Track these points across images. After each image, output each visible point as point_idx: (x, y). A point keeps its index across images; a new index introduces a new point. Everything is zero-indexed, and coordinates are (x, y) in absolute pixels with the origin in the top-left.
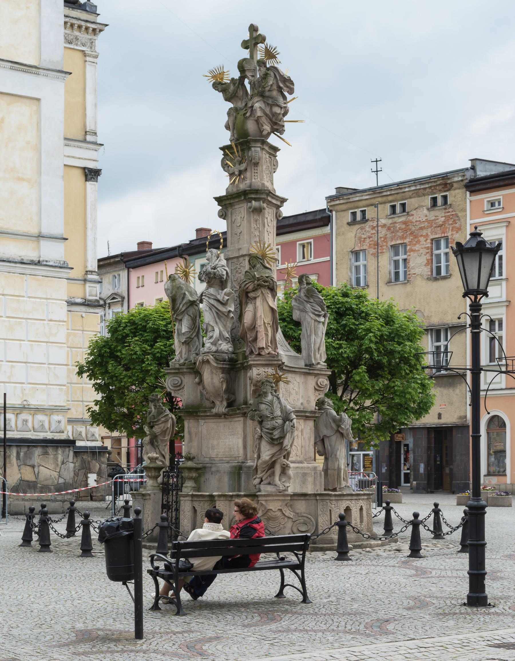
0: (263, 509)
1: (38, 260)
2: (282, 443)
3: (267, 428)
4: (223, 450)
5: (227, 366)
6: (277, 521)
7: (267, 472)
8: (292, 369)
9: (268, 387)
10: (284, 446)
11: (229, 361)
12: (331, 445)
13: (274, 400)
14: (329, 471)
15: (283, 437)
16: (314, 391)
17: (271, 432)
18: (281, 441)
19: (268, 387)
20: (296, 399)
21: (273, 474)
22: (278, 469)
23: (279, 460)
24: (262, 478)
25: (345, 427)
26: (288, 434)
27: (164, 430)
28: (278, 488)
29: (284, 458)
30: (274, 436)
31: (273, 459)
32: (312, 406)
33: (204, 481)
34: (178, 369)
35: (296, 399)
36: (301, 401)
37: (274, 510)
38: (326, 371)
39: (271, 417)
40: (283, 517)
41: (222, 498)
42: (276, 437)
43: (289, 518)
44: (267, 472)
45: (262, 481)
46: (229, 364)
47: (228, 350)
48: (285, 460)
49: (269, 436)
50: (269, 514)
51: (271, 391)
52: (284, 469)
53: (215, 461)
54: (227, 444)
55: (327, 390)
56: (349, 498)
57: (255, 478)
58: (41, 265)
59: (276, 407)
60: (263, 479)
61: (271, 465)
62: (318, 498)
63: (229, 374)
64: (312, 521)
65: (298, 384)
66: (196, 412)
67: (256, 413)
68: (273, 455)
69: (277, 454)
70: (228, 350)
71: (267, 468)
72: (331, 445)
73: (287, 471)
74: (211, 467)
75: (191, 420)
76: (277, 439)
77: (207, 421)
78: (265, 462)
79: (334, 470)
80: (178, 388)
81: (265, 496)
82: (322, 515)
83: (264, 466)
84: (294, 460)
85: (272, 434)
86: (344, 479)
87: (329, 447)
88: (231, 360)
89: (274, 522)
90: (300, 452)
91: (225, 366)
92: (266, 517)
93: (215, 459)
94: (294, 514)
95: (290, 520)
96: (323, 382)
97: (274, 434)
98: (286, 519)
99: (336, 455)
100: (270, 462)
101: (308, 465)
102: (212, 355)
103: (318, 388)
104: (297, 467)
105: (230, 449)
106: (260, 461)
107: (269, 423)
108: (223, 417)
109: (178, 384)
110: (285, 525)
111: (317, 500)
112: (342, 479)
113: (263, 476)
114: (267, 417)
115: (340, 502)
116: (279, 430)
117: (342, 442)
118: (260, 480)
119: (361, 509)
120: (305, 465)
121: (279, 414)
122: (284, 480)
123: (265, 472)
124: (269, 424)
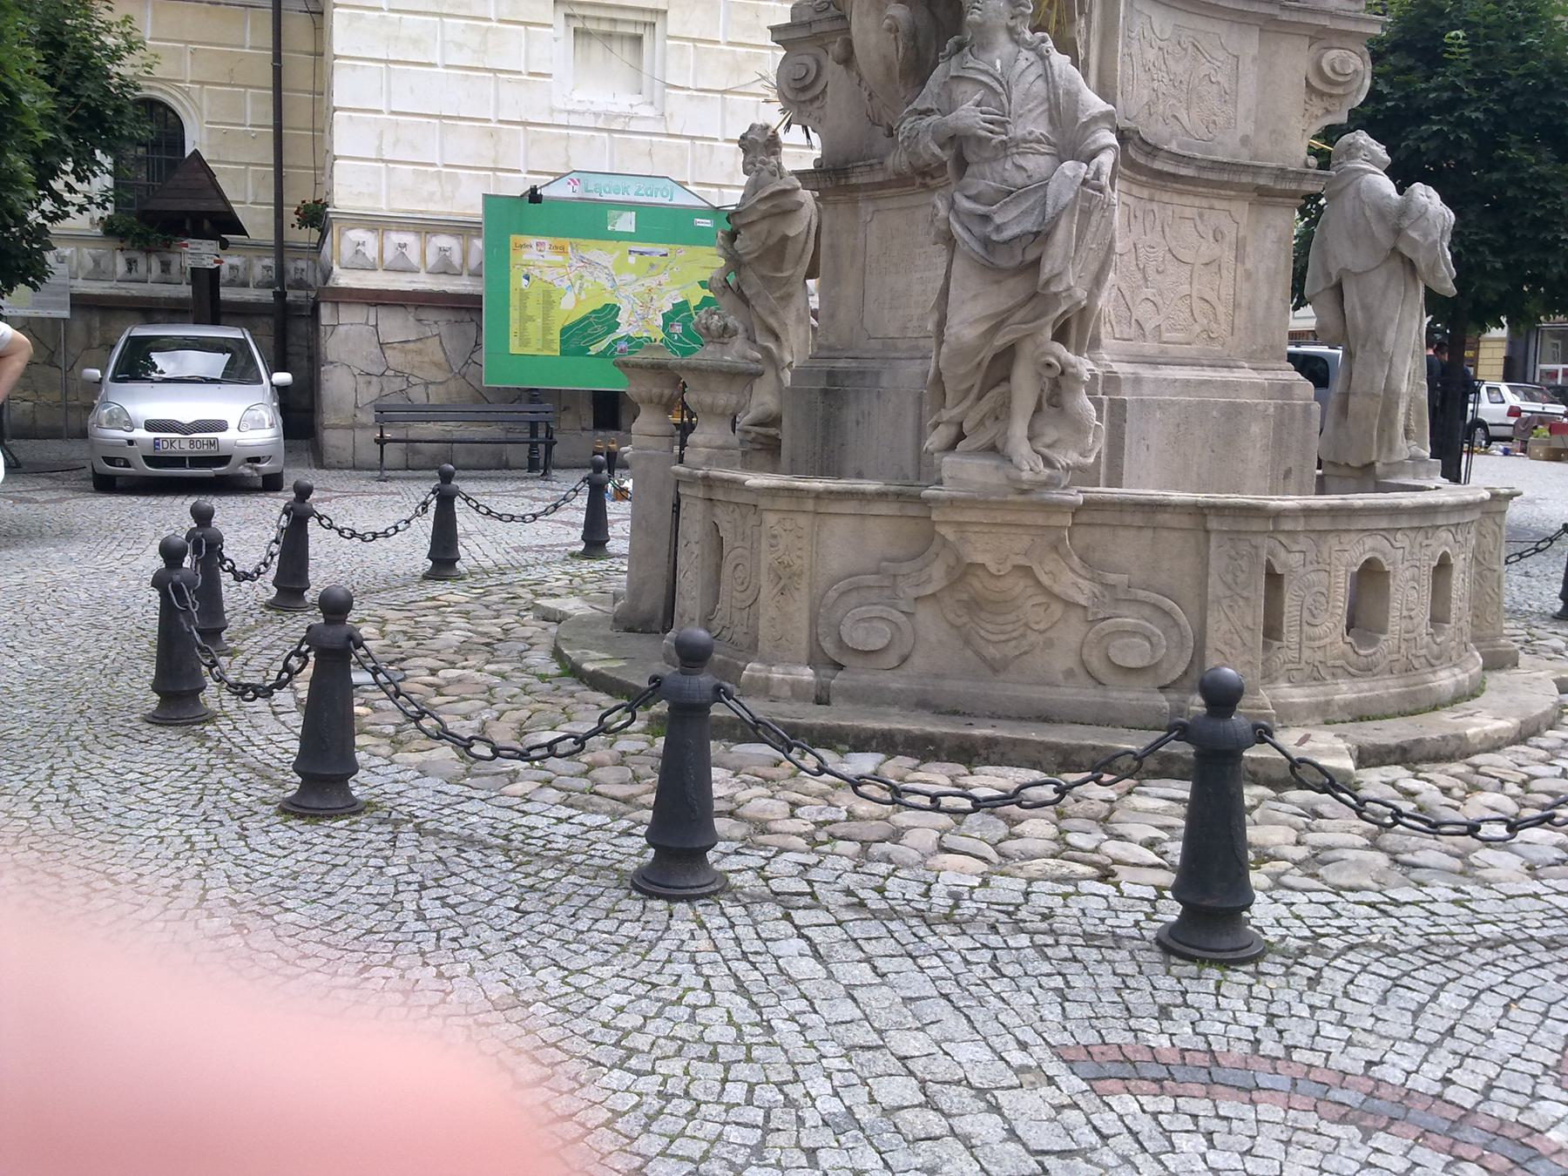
0: (952, 562)
3: (973, 192)
6: (1012, 617)
7: (979, 398)
10: (1044, 276)
12: (1366, 308)
14: (1352, 400)
15: (1041, 236)
16: (1304, 96)
21: (1002, 413)
22: (1024, 387)
23: (1027, 349)
25: (1425, 236)
26: (1063, 223)
27: (771, 242)
28: (1013, 473)
29: (1061, 335)
30: (999, 229)
31: (1001, 341)
32: (1296, 149)
33: (858, 423)
35: (1220, 121)
36: (1246, 127)
37: (993, 569)
38: (1358, 20)
40: (1041, 599)
42: (1007, 234)
43: (1069, 604)
45: (961, 436)
48: (1058, 348)
50: (976, 583)
51: (1006, 19)
52: (1056, 391)
53: (896, 349)
55: (1362, 98)
56: (1384, 523)
57: (936, 426)
59: (1027, 94)
61: (1001, 366)
62: (1213, 524)
64: (1176, 624)
65: (1231, 60)
67: (928, 120)
68: (999, 323)
69: (1018, 316)
71: (978, 380)
72: (1366, 308)
74: (878, 374)
75: (841, 207)
77: (881, 204)
78: (962, 353)
79: (1373, 396)
80: (809, 95)
81: (952, 502)
82: (1225, 603)
83: (962, 370)
84: (1194, 353)
86: (1407, 432)
87: (1359, 313)
89: (1000, 619)
92: (965, 596)
93: (900, 343)
94: (1097, 589)
95: (1075, 618)
96: (1343, 62)
97: (998, 220)
98: (1057, 609)
99: (1380, 343)
100: (987, 354)
101: (1254, 374)
103: (1320, 87)
106: (944, 349)
110: (1050, 634)
111: (1207, 532)
112: (1401, 430)
113: (965, 414)
114: (980, 140)
115: (1332, 541)
117: (1411, 293)
118: (953, 430)
119: (1443, 567)
120: (1245, 375)
121: (1040, 128)
122: (1051, 435)
123: (973, 396)
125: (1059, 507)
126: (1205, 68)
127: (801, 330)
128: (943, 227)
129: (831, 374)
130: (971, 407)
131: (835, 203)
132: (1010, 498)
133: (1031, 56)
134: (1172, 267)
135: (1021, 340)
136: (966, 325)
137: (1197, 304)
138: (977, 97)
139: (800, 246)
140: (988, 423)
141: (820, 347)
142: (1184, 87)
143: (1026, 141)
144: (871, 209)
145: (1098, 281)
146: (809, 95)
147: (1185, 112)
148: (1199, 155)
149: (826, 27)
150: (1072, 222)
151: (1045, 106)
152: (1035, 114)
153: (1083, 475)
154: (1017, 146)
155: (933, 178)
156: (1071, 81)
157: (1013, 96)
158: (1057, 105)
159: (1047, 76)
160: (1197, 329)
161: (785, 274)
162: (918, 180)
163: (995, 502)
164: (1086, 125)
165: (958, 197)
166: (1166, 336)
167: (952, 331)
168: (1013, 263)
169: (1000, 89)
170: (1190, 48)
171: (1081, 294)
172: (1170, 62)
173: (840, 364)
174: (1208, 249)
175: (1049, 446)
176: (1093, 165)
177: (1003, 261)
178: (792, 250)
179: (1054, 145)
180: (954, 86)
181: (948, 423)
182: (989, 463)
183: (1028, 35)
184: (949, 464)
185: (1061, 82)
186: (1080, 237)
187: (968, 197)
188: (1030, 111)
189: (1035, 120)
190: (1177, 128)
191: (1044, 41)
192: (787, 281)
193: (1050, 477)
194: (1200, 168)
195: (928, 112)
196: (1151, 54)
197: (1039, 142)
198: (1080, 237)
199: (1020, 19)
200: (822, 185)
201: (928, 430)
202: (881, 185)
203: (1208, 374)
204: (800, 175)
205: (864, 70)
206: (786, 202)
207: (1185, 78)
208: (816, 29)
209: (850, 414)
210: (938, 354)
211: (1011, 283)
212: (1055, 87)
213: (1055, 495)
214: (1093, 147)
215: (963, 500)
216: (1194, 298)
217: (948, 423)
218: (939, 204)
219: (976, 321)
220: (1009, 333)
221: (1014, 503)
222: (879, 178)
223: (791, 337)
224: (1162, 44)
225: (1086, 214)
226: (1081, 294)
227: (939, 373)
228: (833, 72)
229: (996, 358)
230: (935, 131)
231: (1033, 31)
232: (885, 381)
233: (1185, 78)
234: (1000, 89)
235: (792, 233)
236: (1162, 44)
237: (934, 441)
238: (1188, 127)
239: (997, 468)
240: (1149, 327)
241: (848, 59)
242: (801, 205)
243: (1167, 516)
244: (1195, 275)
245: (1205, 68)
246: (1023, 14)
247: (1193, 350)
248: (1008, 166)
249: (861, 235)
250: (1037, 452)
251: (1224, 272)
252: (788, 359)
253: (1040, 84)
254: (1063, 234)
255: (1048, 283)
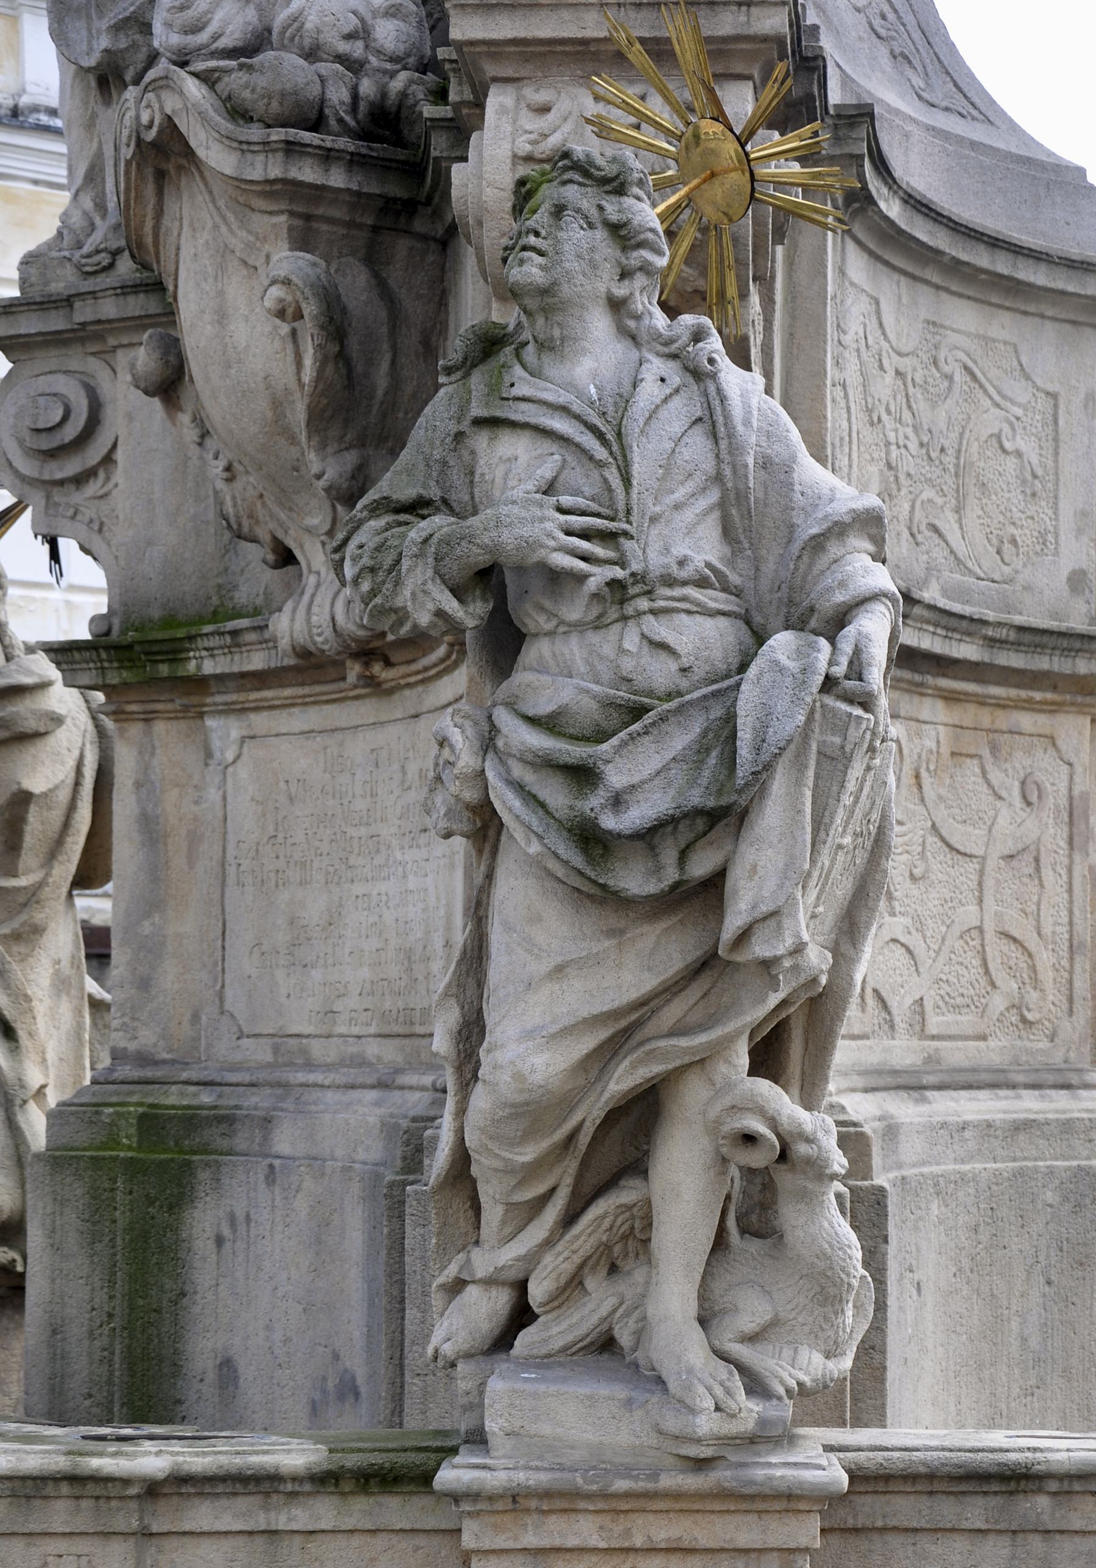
1: (10, 103)
2: (712, 890)
3: (543, 707)
4: (365, 973)
5: (338, 178)
7: (569, 1219)
8: (981, 258)
9: (576, 236)
10: (734, 922)
11: (363, 135)
13: (649, 391)
15: (723, 817)
17: (576, 752)
18: (701, 866)
19: (576, 236)
20: (1026, 536)
21: (632, 1243)
22: (683, 1185)
23: (693, 1102)
24: (521, 1287)
26: (778, 786)
28: (672, 1423)
29: (767, 1058)
30: (617, 802)
31: (624, 1079)
34: (67, 302)
35: (1026, 536)
39: (599, 576)
41: (59, 1514)
42: (638, 815)
44: (569, 1219)
45: (522, 1315)
46: (355, 161)
47: (362, 33)
48: (764, 1086)
49: (556, 794)
51: (606, 282)
53: (310, 1065)
54: (389, 916)
57: (457, 1286)
58: (22, 127)
59: (668, 465)
60: (537, 1292)
63: (373, 259)
65: (1043, 404)
66: (175, 651)
67: (419, 530)
68: (624, 1030)
69: (672, 1013)
70: (362, 33)
71: (565, 1175)
73: (790, 1216)
74: (267, 1121)
76: (648, 837)
77: (260, 721)
78: (531, 1113)
80: (71, 467)
81: (515, 1501)
83: (527, 1154)
85: (583, 776)
88: (384, 123)
90: (1054, 995)
91: (308, 173)
93: (317, 1049)
97: (616, 777)
100: (591, 1112)
102: (207, 79)
104: (1022, 1127)
105: (408, 956)
106: (480, 1100)
107: (573, 649)
108: (354, 671)
109: (70, 432)
113: (533, 1259)
114: (557, 580)
116: (681, 738)
118: (501, 1301)
121: (704, 549)
122: (751, 1310)
123: (552, 1214)
124: (564, 670)
125: (789, 1500)
126: (991, 420)
127: (65, 1009)
128: (470, 795)
129: (151, 1123)
130: (548, 1243)
131: (148, 718)
132: (668, 1481)
133: (672, 371)
134: (939, 863)
135: (679, 1072)
136: (531, 1047)
137: (996, 950)
138: (546, 472)
139: (56, 816)
140: (590, 1283)
141: (118, 1055)
142: (949, 460)
143: (670, 581)
144: (235, 734)
145: (849, 928)
146: (71, 467)
147: (951, 517)
148: (991, 616)
149: (109, 308)
150: (799, 783)
151: (714, 496)
152: (689, 515)
153: (821, 1403)
154: (649, 593)
155: (388, 664)
156: (770, 434)
157: (636, 470)
158: (741, 496)
159: (712, 420)
160: (998, 1003)
161: (22, 882)
162: (354, 671)
163: (628, 1495)
164: (817, 544)
165: (504, 718)
166: (935, 1022)
167: (502, 1056)
168: (652, 887)
169: (601, 453)
170: (959, 376)
171: (818, 959)
172: (921, 405)
173: (173, 1097)
174: (1012, 824)
175: (751, 1339)
176: (848, 636)
177: (634, 879)
178: (37, 826)
179: (738, 593)
180: (481, 440)
181: (489, 1282)
182: (610, 1391)
183: (660, 320)
184: (507, 1397)
185: (751, 439)
186: (820, 824)
187: (533, 721)
188: (677, 507)
189: (690, 530)
190: (939, 554)
191: (698, 336)
192: (32, 896)
193: (763, 1422)
194: (992, 643)
195: (418, 507)
196: (885, 387)
197: (702, 583)
198: (820, 824)
199: (640, 280)
200: (113, 678)
201: (437, 1300)
202: (260, 679)
203: (1030, 1104)
204: (63, 653)
205: (217, 411)
206: (22, 710)
207: (950, 442)
208: (83, 313)
209: (203, 1220)
210: (461, 1112)
211: (648, 935)
212: (736, 448)
213: (776, 1468)
214: (840, 597)
215: (547, 1494)
216: (990, 935)
217: (489, 1282)
218: (456, 737)
219: (566, 1031)
220: (640, 1062)
221: (677, 1495)
222: (257, 661)
223: (42, 1025)
224: (905, 364)
225: (834, 762)
226: (818, 959)
227: (462, 1158)
228: (133, 417)
229: (613, 1116)
230: (440, 553)
231: (671, 311)
232: (286, 1140)
233: (950, 442)
234: (601, 453)
235: (36, 784)
236: (905, 364)
237: (459, 1323)
238: (961, 550)
239: (629, 1403)
240: (901, 1005)
241: (170, 384)
242: (58, 720)
243: (1043, 1502)
244: (989, 883)
245: (991, 420)
246: (646, 269)
247: (994, 1051)
248: (632, 641)
249: (213, 795)
250: (724, 1357)
251: (1047, 874)
252: (34, 1077)
253: (698, 440)
254: (777, 816)
255: (743, 937)
